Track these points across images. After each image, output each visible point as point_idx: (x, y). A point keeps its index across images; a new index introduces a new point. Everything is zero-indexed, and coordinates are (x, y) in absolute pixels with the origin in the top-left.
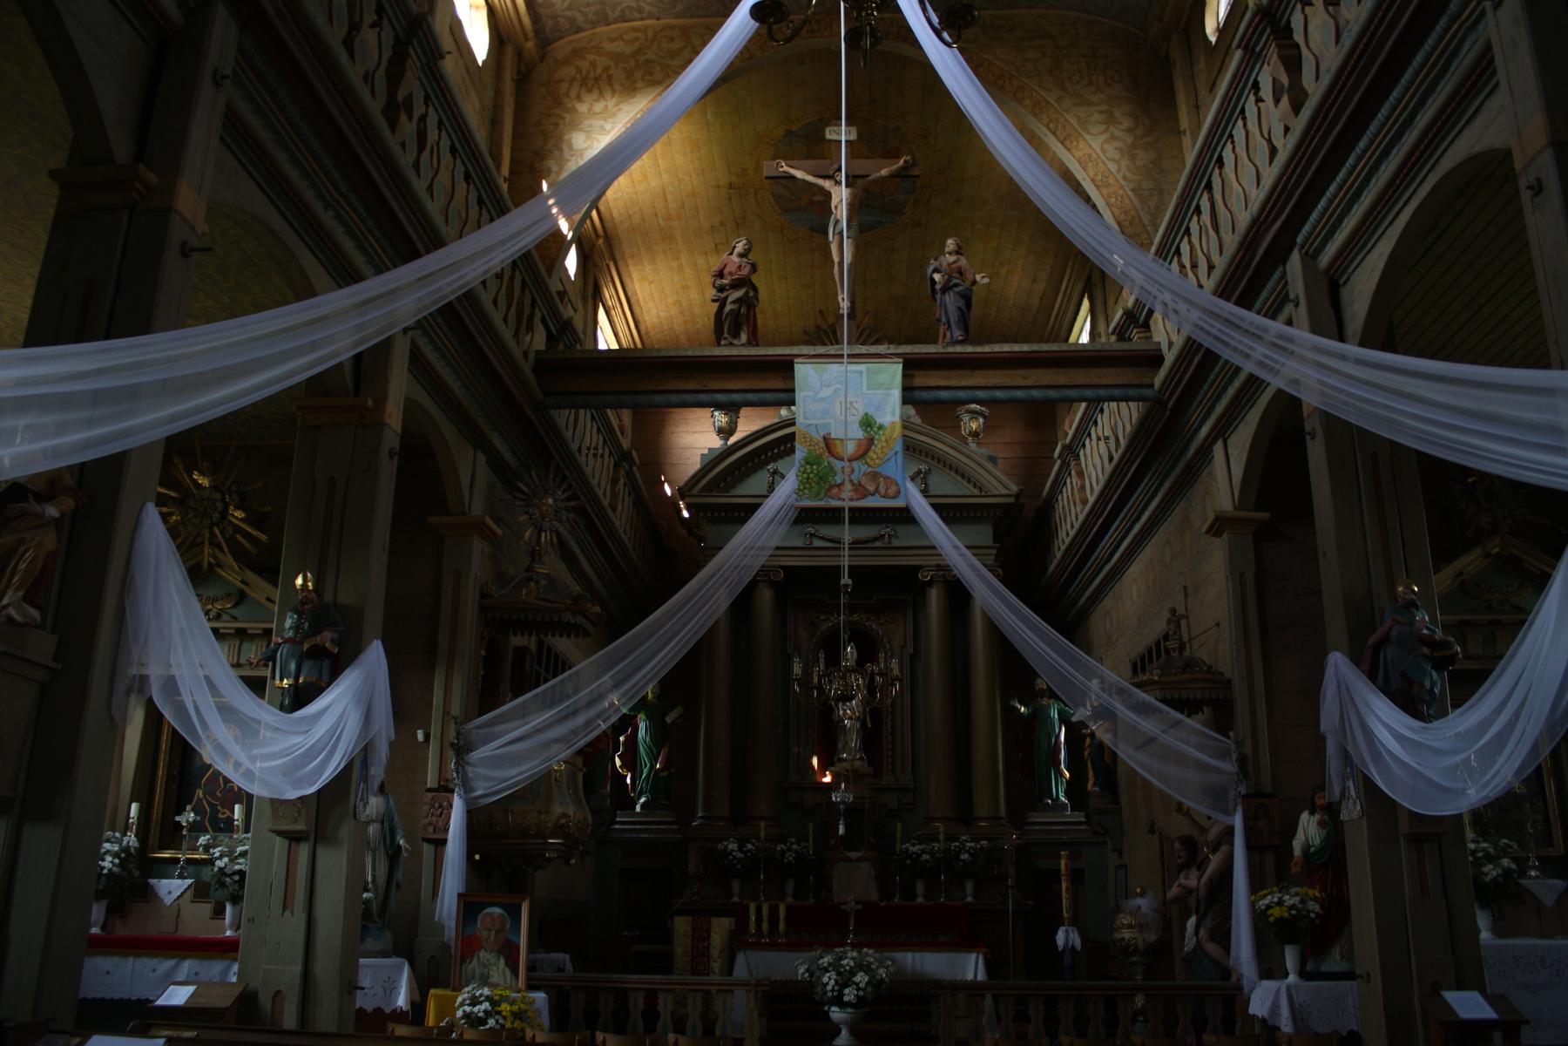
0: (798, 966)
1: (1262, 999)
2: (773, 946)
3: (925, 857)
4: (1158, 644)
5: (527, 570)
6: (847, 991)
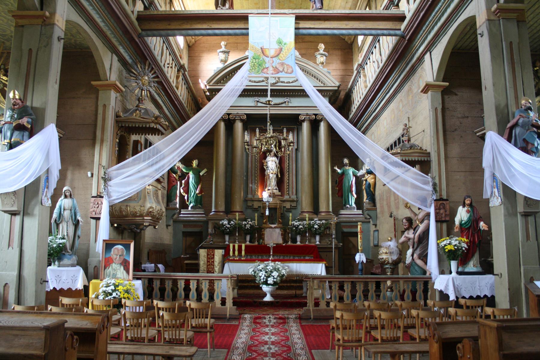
0: (247, 269)
1: (442, 283)
2: (240, 261)
3: (301, 227)
4: (399, 139)
5: (136, 107)
6: (269, 279)
